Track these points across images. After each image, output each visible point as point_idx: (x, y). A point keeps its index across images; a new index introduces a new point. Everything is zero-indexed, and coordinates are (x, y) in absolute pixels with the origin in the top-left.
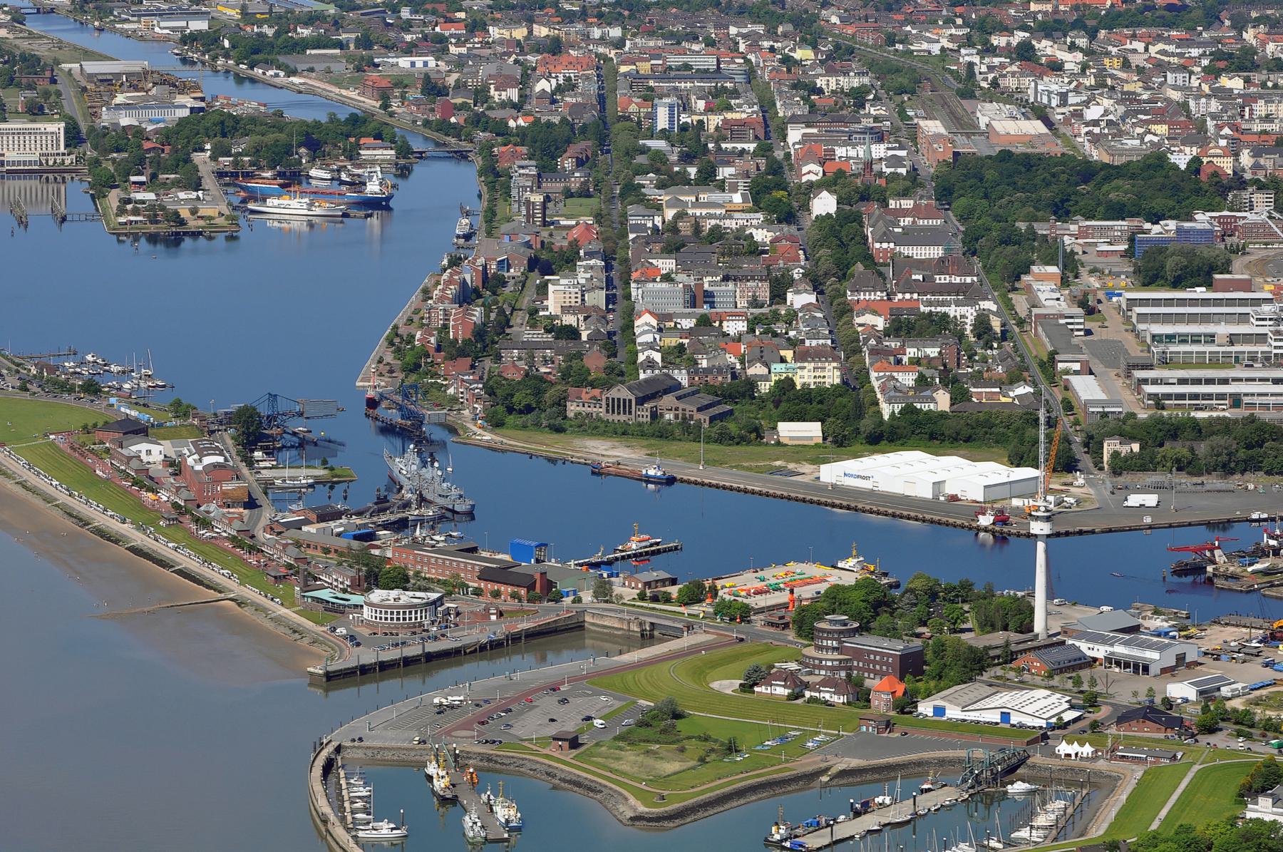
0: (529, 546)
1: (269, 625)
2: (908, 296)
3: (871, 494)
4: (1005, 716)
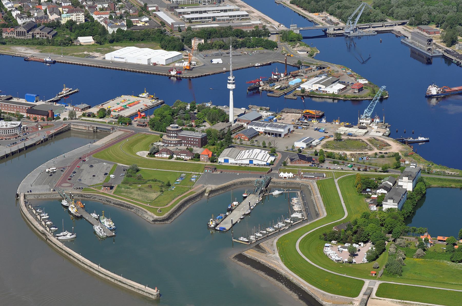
0: (33, 96)
3: (125, 64)
4: (251, 162)
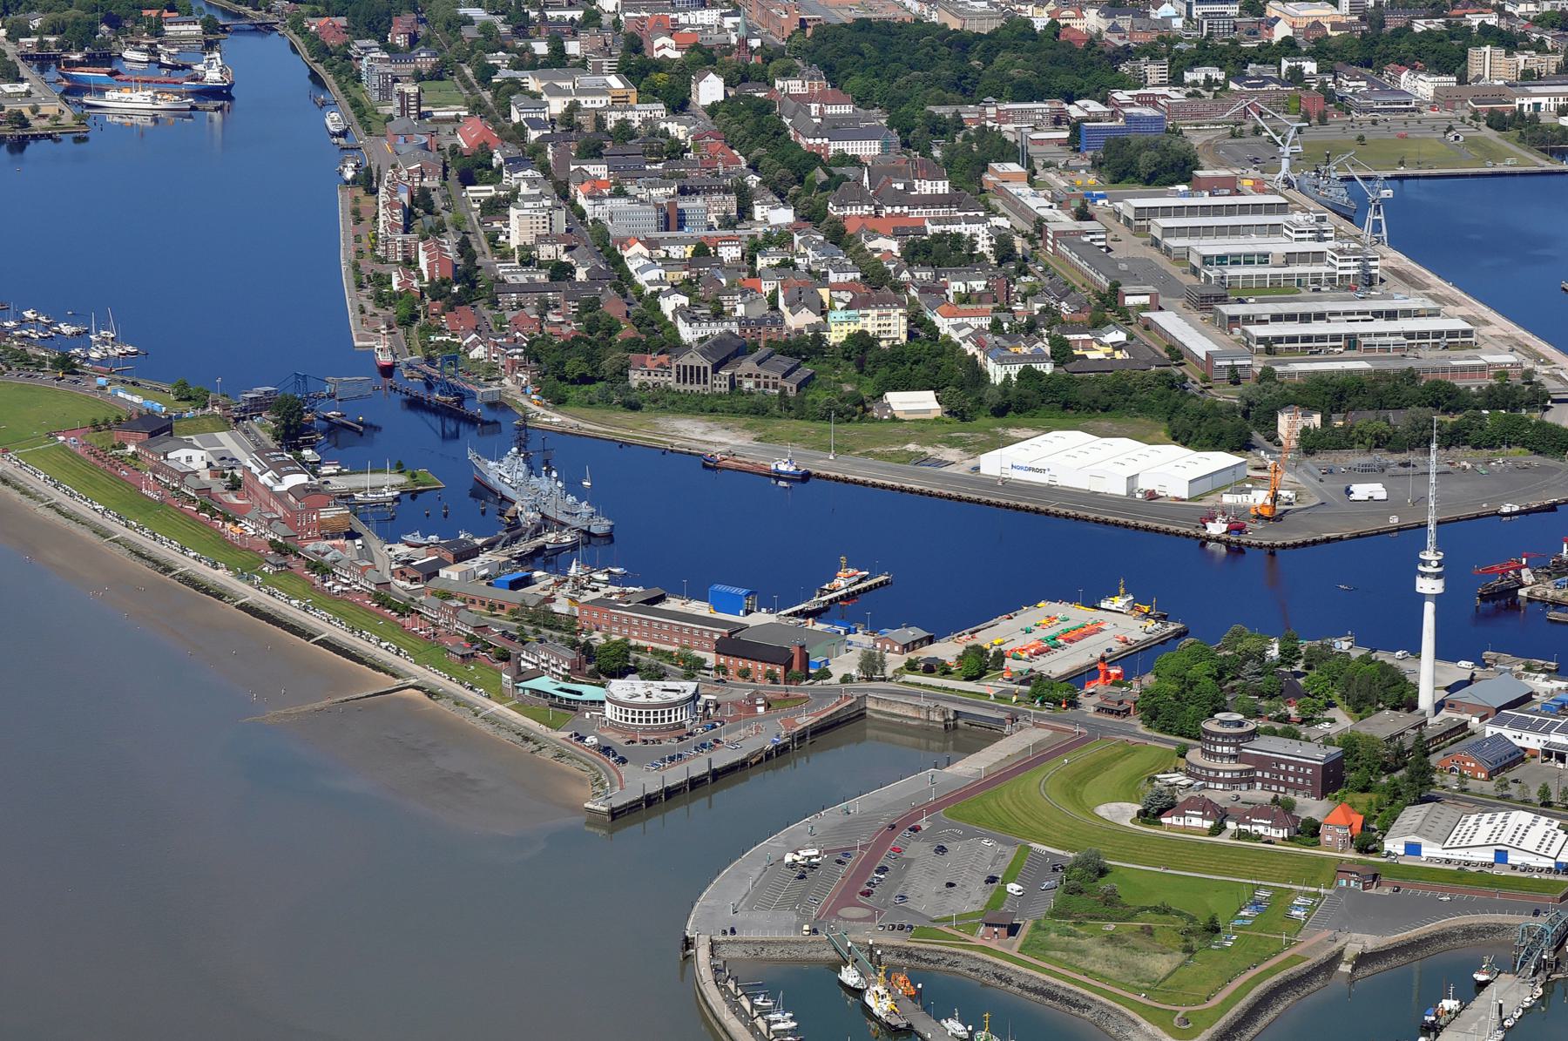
0: (736, 595)
1: (487, 728)
2: (897, 210)
